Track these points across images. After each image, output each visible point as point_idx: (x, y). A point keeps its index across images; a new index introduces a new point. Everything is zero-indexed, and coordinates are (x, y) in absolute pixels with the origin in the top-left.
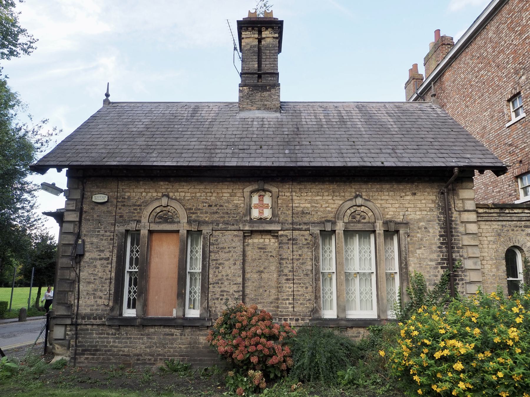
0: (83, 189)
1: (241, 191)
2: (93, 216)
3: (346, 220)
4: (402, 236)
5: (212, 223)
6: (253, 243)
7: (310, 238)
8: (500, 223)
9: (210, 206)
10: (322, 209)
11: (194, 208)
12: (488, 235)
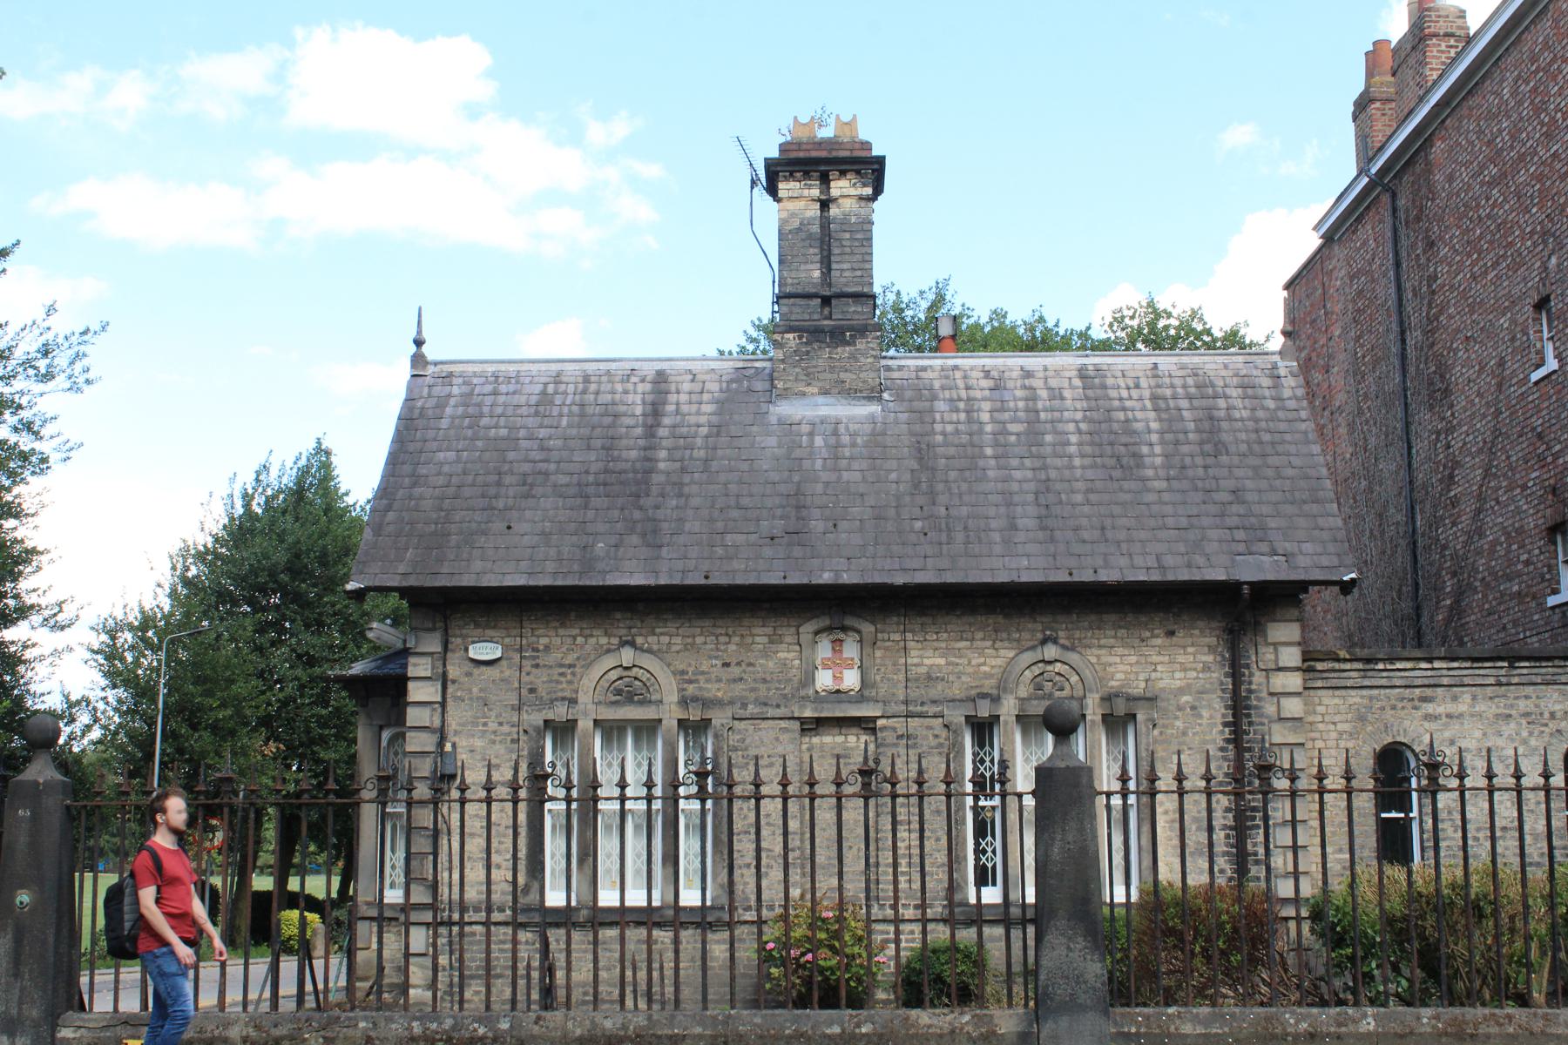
0: (446, 630)
1: (793, 630)
2: (470, 690)
3: (1023, 692)
4: (1142, 727)
5: (731, 703)
6: (822, 745)
7: (944, 733)
8: (1365, 692)
9: (726, 665)
10: (970, 670)
11: (690, 670)
12: (1337, 718)
